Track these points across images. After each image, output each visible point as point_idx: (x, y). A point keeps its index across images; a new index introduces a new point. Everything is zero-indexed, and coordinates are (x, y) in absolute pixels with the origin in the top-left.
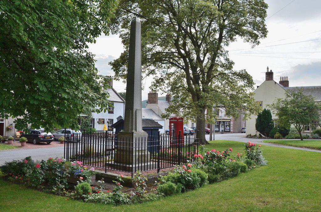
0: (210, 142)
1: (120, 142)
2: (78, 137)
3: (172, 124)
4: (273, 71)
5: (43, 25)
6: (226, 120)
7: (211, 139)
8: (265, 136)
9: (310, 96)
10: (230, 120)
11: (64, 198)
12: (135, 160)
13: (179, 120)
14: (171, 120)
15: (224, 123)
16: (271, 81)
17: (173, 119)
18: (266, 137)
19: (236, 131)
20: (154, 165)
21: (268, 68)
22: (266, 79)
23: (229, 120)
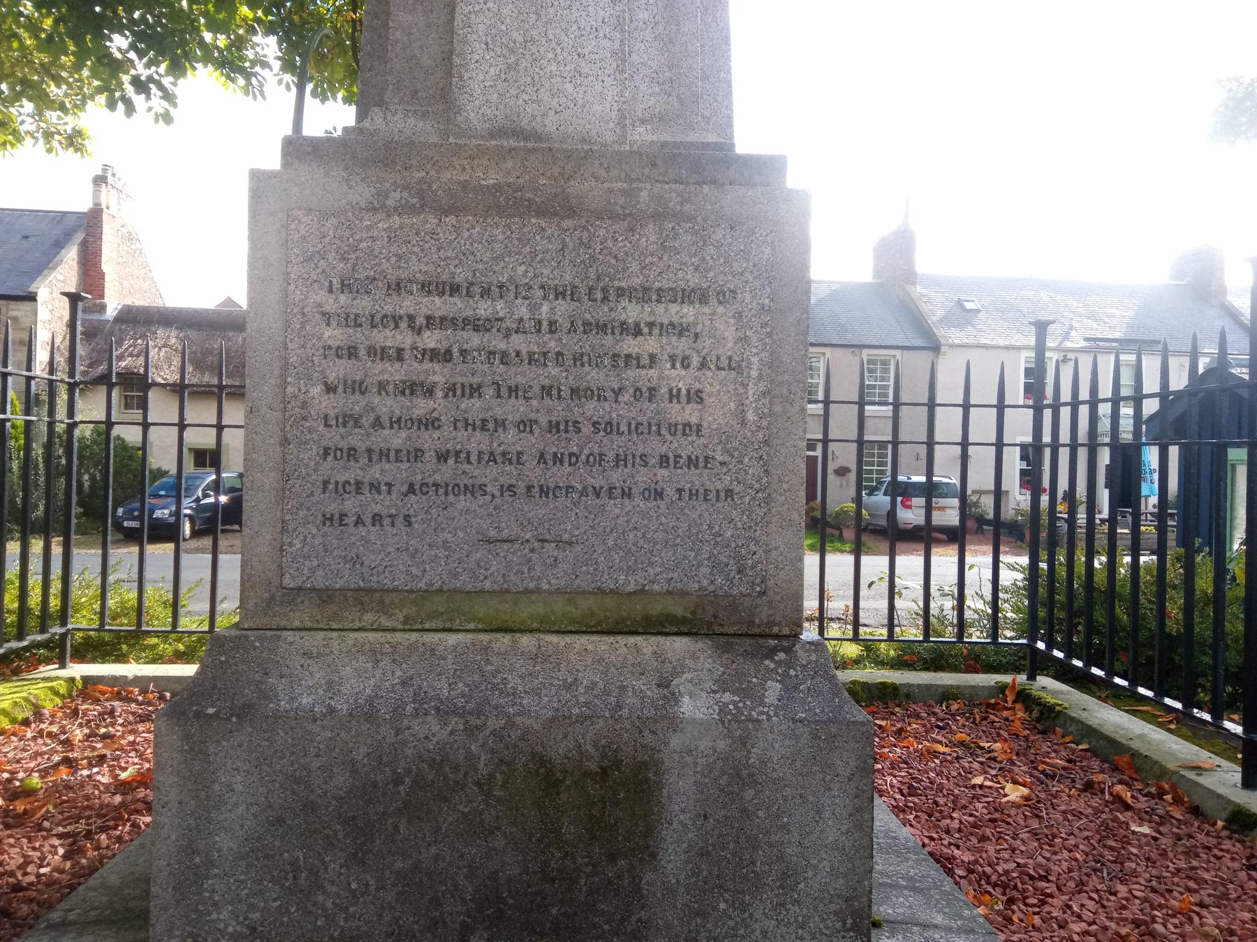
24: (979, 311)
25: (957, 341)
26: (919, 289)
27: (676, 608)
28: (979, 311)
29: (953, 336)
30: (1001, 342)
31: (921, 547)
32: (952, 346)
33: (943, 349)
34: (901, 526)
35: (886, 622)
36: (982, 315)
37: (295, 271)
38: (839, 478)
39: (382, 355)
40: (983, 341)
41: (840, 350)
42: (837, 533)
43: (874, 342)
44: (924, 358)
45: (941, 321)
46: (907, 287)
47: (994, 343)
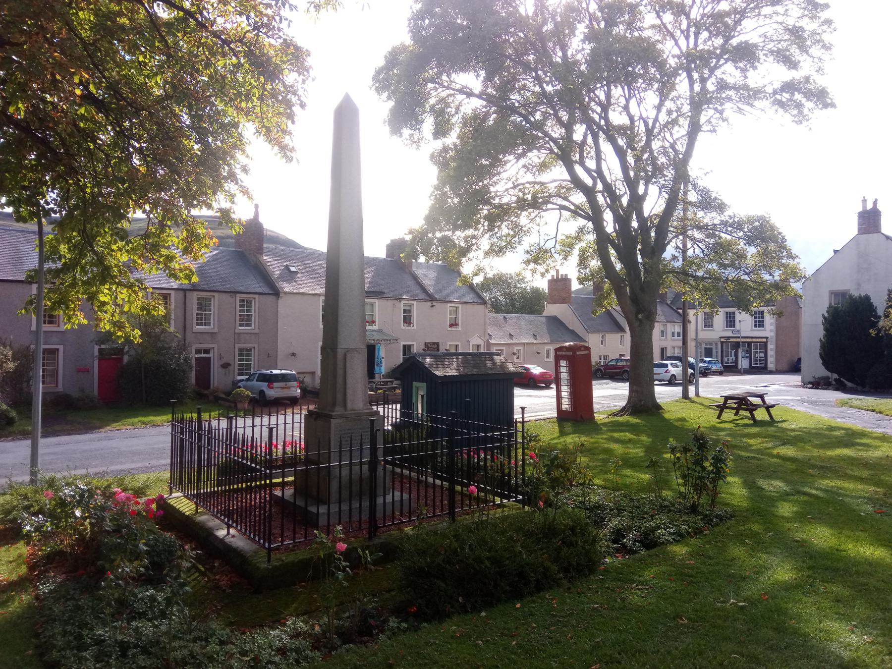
0: (696, 399)
1: (340, 465)
2: (244, 504)
3: (563, 363)
4: (879, 207)
5: (162, 169)
6: (754, 340)
7: (697, 395)
8: (858, 384)
9: (562, 433)
10: (767, 338)
11: (36, 492)
12: (382, 484)
13: (578, 353)
14: (558, 353)
15: (748, 347)
16: (875, 235)
17: (564, 349)
18: (859, 388)
19: (785, 366)
20: (404, 502)
21: (864, 201)
22: (859, 230)
23: (765, 340)
24: (298, 272)
25: (288, 291)
26: (265, 257)
27: (819, 463)
28: (298, 272)
29: (287, 287)
30: (310, 292)
31: (171, 408)
32: (286, 293)
33: (281, 295)
34: (268, 399)
35: (343, 454)
36: (299, 275)
37: (459, 120)
38: (224, 370)
39: (130, 270)
40: (302, 291)
41: (224, 294)
42: (233, 405)
43: (243, 290)
44: (271, 298)
45: (278, 277)
46: (258, 256)
47: (307, 292)
